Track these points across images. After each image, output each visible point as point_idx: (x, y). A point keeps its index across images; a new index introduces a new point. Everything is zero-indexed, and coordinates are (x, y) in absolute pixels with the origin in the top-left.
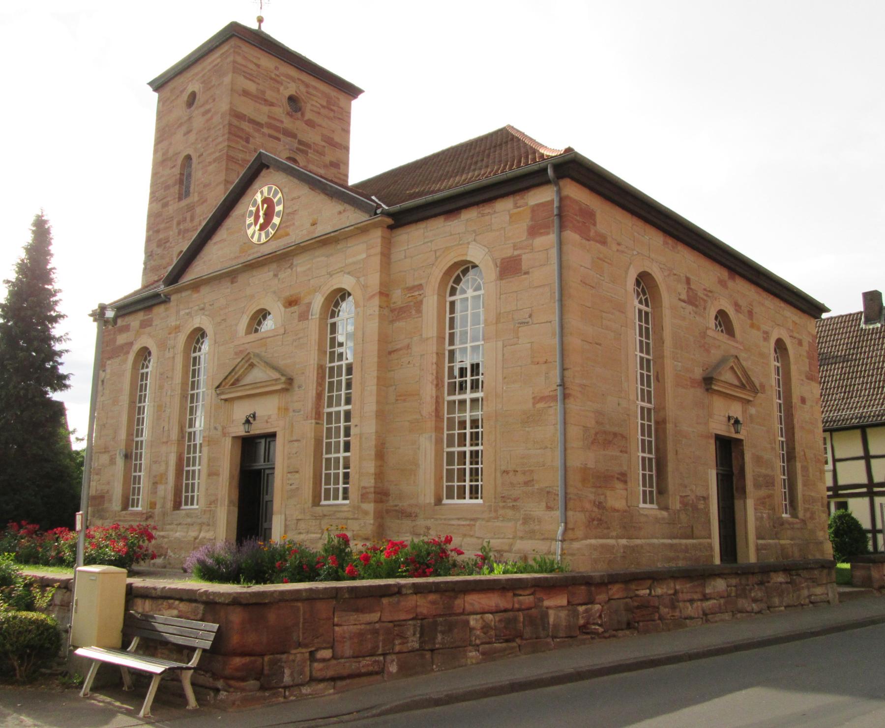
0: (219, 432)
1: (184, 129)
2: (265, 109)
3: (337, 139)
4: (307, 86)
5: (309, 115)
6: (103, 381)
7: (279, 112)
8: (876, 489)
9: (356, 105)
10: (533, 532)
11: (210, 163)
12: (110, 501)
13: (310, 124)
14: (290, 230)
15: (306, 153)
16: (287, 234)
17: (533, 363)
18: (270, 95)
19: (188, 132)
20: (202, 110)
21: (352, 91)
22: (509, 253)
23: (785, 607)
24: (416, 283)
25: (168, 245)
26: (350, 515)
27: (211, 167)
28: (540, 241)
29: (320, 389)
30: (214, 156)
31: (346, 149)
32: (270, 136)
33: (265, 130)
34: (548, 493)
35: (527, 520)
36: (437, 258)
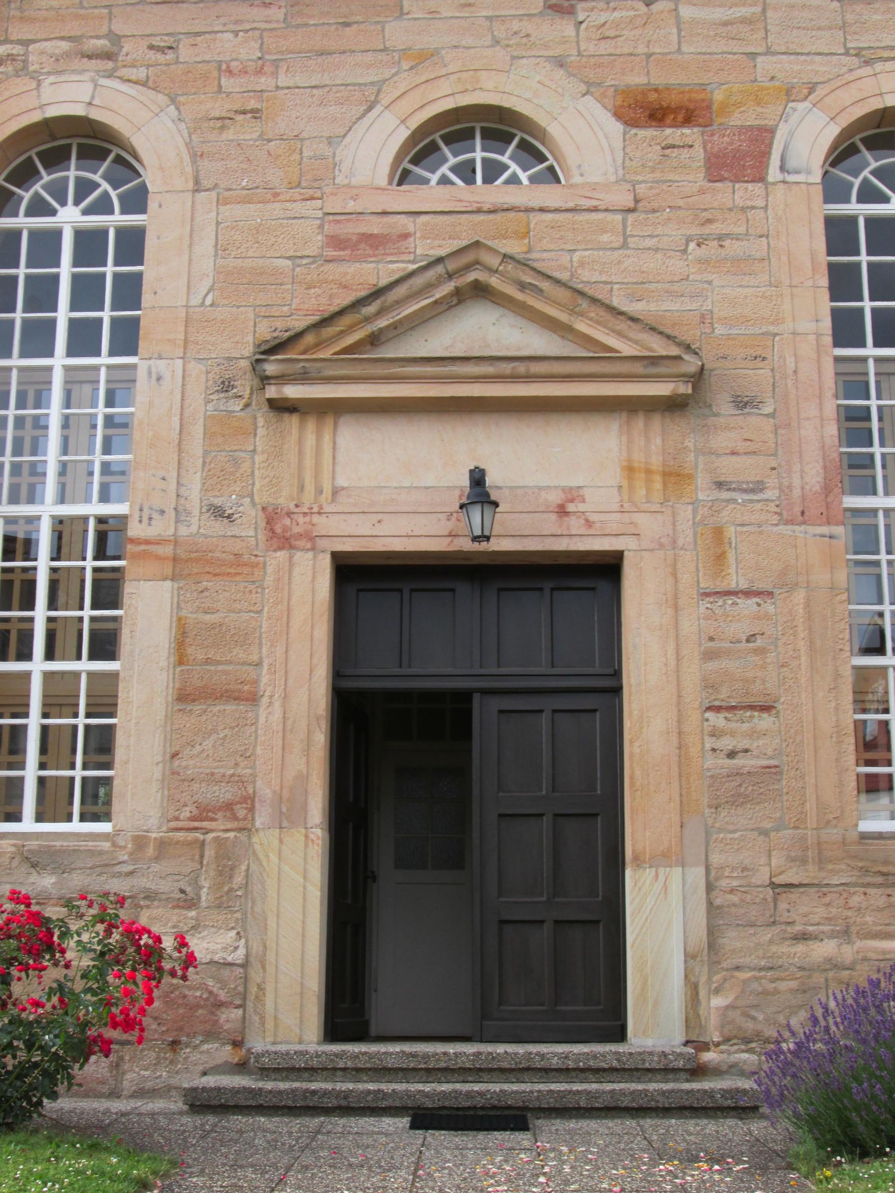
0: (248, 528)
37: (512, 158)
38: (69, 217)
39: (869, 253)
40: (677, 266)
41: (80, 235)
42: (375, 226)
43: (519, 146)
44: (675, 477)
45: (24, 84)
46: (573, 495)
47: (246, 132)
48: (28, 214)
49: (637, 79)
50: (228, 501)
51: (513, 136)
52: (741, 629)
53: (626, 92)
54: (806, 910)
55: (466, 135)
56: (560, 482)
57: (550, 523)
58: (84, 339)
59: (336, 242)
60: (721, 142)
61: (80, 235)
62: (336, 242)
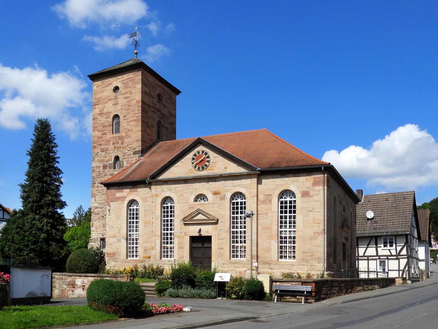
0: (183, 234)
1: (113, 102)
2: (151, 99)
3: (172, 112)
4: (163, 89)
5: (164, 102)
6: (109, 210)
7: (155, 100)
8: (360, 258)
9: (178, 98)
10: (314, 269)
11: (131, 121)
12: (120, 255)
13: (164, 106)
14: (214, 168)
15: (163, 118)
16: (213, 170)
17: (313, 223)
18: (152, 93)
19: (116, 104)
20: (124, 96)
21: (177, 92)
22: (305, 189)
23: (181, 311)
24: (269, 194)
25: (108, 152)
26: (247, 263)
27: (132, 123)
28: (316, 188)
29: (287, 231)
30: (133, 119)
31: (175, 117)
32: (153, 111)
33: (152, 109)
34: (318, 258)
35: (311, 266)
36: (277, 187)
40: (217, 209)
42: (192, 206)
44: (216, 229)
45: (164, 193)
46: (208, 231)
47: (182, 197)
49: (214, 190)
50: (182, 231)
52: (221, 242)
53: (213, 191)
54: (225, 266)
56: (206, 231)
57: (206, 233)
58: (290, 212)
59: (189, 208)
60: (221, 196)
62: (189, 208)
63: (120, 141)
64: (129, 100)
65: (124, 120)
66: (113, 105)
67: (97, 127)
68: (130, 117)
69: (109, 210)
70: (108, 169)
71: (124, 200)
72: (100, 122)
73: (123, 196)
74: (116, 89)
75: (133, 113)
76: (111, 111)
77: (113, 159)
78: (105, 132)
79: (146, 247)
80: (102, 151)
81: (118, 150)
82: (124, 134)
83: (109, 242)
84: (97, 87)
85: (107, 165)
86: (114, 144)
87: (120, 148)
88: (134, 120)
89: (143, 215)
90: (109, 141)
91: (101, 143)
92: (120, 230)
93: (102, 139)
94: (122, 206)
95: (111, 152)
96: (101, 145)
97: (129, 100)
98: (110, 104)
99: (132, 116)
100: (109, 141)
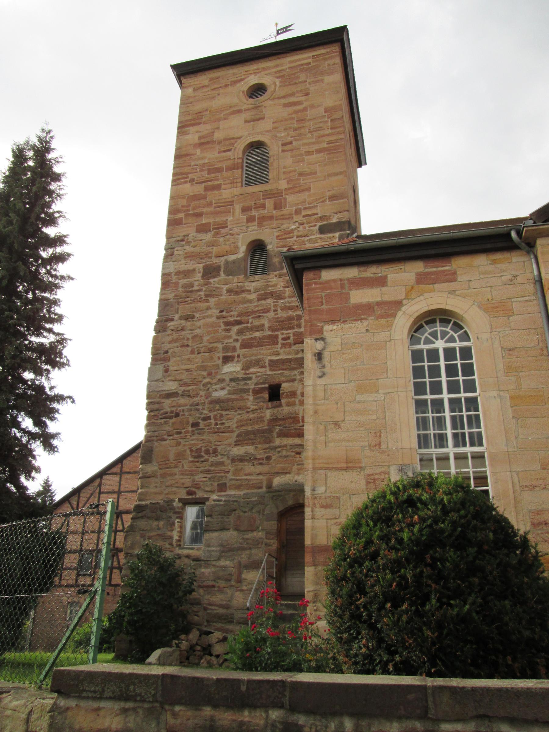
11: (309, 153)
25: (223, 231)
37: (451, 329)
38: (440, 345)
39: (425, 382)
41: (446, 350)
43: (453, 324)
48: (425, 343)
51: (451, 320)
55: (433, 321)
61: (446, 350)
63: (270, 203)
64: (300, 107)
65: (283, 151)
66: (246, 122)
67: (187, 174)
68: (304, 144)
69: (319, 356)
70: (223, 276)
71: (394, 316)
72: (201, 162)
73: (387, 298)
74: (258, 90)
75: (315, 134)
76: (237, 135)
77: (243, 249)
78: (216, 183)
79: (539, 512)
80: (202, 229)
81: (260, 225)
82: (283, 185)
83: (321, 490)
84: (194, 90)
85: (219, 267)
86: (245, 210)
87: (271, 218)
88: (319, 151)
89: (501, 366)
90: (231, 203)
91: (199, 210)
92: (378, 434)
93: (203, 202)
94: (382, 336)
95: (235, 231)
96: (200, 215)
97: (300, 107)
98: (237, 121)
99: (314, 140)
100: (231, 203)
